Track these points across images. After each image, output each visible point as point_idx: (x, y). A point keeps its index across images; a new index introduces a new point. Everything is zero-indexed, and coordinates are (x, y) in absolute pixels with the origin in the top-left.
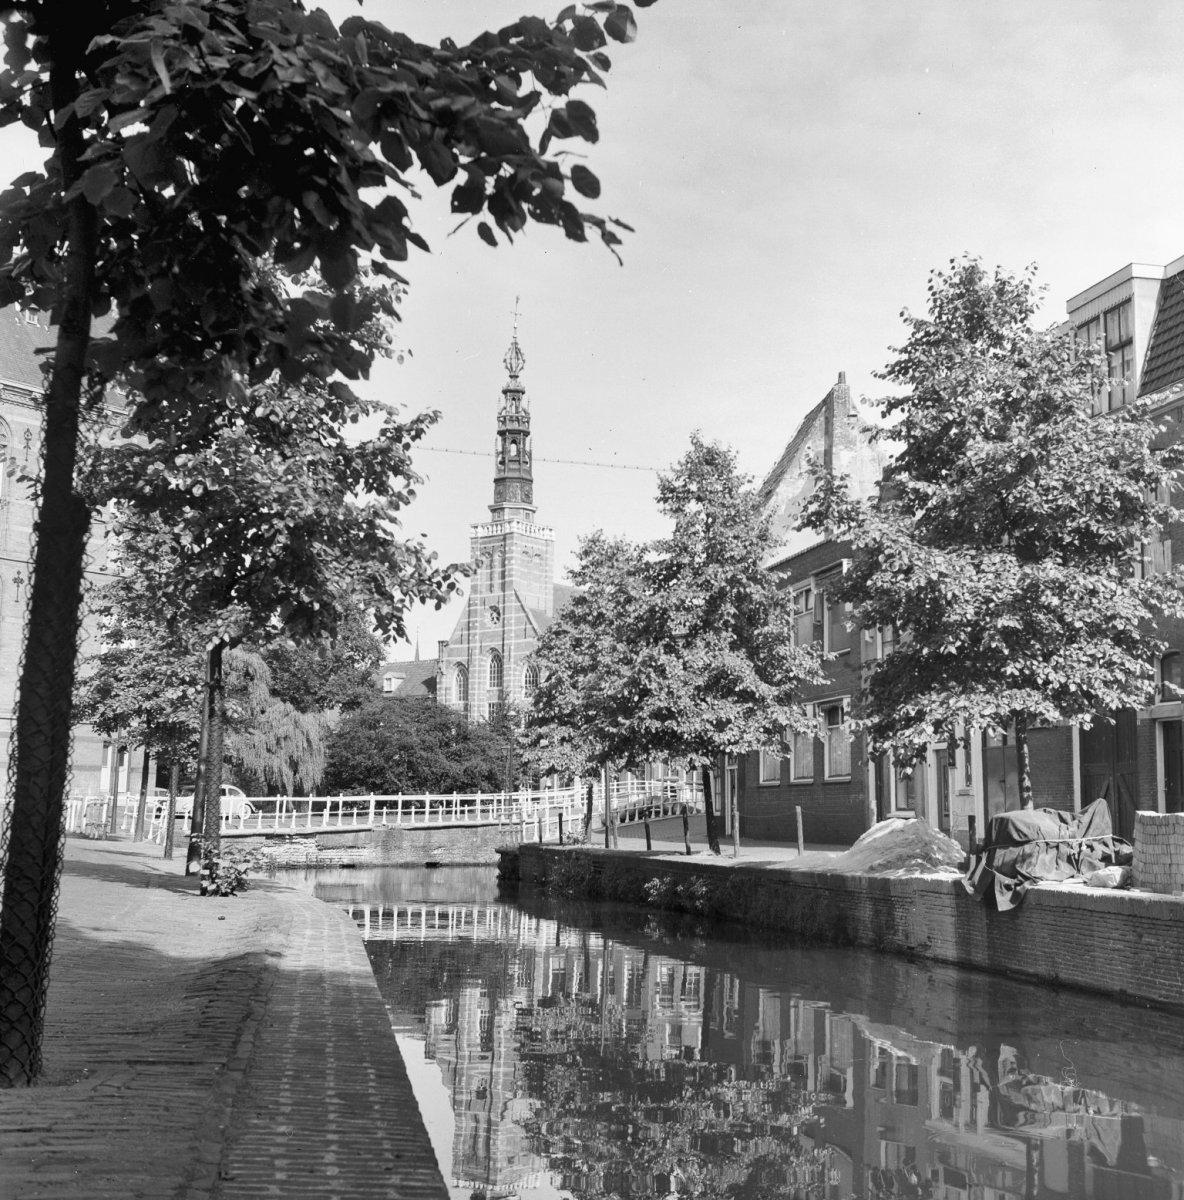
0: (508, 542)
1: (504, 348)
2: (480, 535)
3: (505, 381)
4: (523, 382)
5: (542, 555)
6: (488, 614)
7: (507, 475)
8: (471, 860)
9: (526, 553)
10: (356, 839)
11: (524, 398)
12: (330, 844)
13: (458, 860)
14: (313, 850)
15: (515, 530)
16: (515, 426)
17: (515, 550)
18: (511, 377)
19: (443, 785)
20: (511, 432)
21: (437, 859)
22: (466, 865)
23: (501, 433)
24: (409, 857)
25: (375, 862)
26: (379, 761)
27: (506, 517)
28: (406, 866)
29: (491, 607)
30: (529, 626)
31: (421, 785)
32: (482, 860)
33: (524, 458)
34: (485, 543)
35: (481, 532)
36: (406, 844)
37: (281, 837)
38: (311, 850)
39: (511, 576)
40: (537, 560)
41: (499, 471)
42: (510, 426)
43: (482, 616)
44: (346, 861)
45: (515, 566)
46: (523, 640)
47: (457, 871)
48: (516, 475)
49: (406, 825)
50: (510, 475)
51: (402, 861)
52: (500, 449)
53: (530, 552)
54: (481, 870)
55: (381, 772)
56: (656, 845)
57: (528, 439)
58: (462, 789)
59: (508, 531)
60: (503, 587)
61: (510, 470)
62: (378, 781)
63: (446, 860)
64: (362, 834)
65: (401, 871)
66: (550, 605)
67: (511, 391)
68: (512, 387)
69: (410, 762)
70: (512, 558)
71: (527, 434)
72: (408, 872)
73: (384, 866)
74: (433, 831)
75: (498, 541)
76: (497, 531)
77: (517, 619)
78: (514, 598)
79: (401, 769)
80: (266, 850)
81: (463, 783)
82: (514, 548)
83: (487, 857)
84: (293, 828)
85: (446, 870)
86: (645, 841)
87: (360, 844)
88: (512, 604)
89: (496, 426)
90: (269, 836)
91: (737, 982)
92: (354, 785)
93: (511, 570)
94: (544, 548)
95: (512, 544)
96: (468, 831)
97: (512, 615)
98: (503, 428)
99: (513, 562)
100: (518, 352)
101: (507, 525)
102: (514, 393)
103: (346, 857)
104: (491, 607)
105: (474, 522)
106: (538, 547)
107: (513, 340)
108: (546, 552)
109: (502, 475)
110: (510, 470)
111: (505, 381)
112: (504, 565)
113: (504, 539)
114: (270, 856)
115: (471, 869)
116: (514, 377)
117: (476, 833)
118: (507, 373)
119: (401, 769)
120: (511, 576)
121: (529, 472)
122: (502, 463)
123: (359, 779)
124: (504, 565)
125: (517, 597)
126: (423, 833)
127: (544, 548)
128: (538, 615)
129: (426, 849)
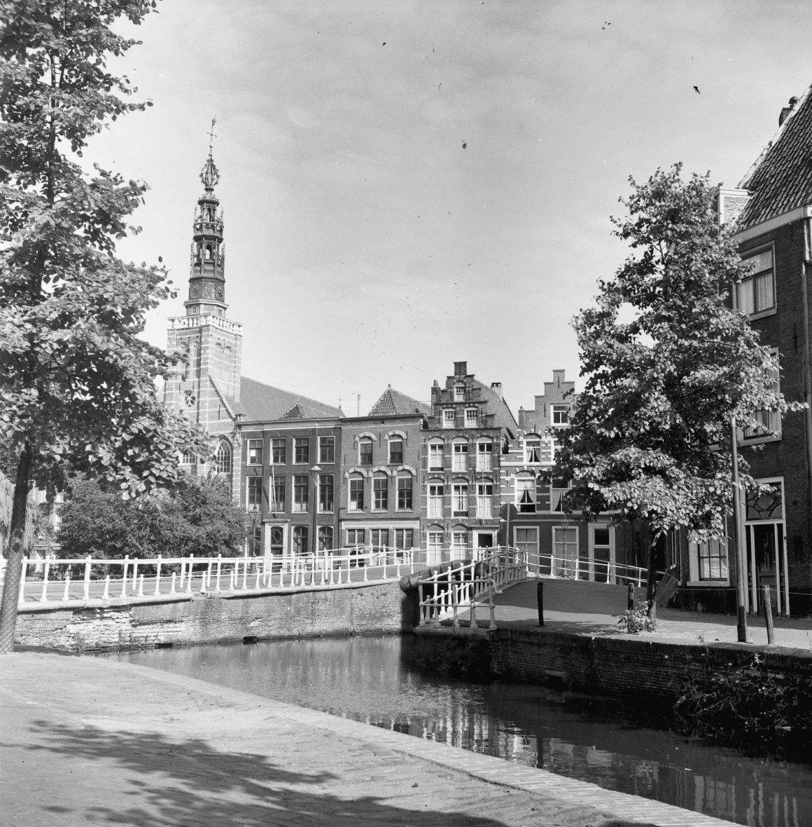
0: (204, 333)
1: (200, 166)
2: (176, 327)
3: (201, 193)
4: (218, 193)
5: (233, 347)
6: (182, 398)
7: (203, 274)
8: (284, 632)
9: (218, 344)
10: (174, 611)
11: (218, 209)
12: (146, 619)
13: (274, 633)
14: (126, 627)
15: (211, 323)
16: (210, 232)
17: (210, 341)
18: (207, 190)
19: (183, 548)
20: (207, 237)
21: (254, 633)
22: (281, 639)
23: (197, 239)
24: (227, 632)
25: (194, 639)
26: (119, 523)
27: (201, 312)
28: (225, 642)
29: (186, 392)
30: (223, 409)
31: (163, 546)
32: (295, 632)
33: (218, 263)
34: (180, 334)
35: (178, 325)
36: (224, 616)
37: (90, 611)
38: (124, 627)
39: (206, 364)
40: (227, 351)
41: (196, 271)
42: (206, 232)
43: (177, 399)
44: (163, 639)
45: (210, 354)
46: (217, 421)
47: (273, 645)
48: (211, 275)
49: (225, 593)
50: (206, 275)
51: (221, 636)
52: (196, 253)
53: (223, 344)
54: (295, 644)
55: (121, 535)
56: (549, 615)
57: (221, 245)
58: (198, 553)
59: (204, 324)
60: (198, 374)
61: (205, 271)
62: (118, 545)
63: (263, 634)
64: (181, 605)
65: (220, 648)
66: (238, 392)
67: (207, 202)
68: (208, 198)
69: (152, 526)
70: (207, 348)
71: (220, 240)
72: (226, 649)
73: (203, 644)
74: (251, 600)
75: (194, 333)
76: (195, 324)
77: (211, 402)
78: (208, 383)
79: (142, 533)
80: (72, 629)
81: (205, 546)
82: (209, 339)
83: (300, 628)
84: (106, 600)
85: (263, 645)
86: (537, 611)
87: (178, 616)
88: (206, 388)
89: (191, 234)
90: (77, 610)
91: (794, 800)
92: (92, 548)
93: (206, 359)
94: (234, 342)
95: (208, 336)
96: (282, 599)
97: (207, 399)
98: (199, 233)
99: (208, 351)
100: (213, 167)
101: (203, 319)
102: (209, 205)
103: (162, 634)
104: (186, 392)
105: (172, 316)
106: (229, 340)
107: (208, 158)
108: (236, 345)
109: (198, 275)
110: (205, 271)
111: (201, 193)
112: (199, 354)
113: (200, 332)
114: (76, 636)
115: (284, 644)
116: (209, 190)
117: (290, 602)
118: (204, 186)
119: (142, 533)
120: (206, 364)
121: (222, 274)
122: (198, 264)
123: (97, 543)
124: (199, 354)
125: (212, 382)
126: (240, 601)
127: (234, 342)
128: (231, 400)
129: (244, 621)
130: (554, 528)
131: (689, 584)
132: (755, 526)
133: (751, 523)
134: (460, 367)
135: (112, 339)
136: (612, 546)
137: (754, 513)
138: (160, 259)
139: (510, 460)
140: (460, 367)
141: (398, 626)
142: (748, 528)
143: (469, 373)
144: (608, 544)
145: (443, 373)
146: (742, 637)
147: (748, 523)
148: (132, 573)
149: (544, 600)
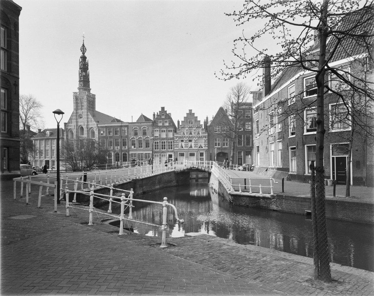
4: (86, 55)
130: (178, 153)
131: (305, 175)
132: (336, 157)
133: (335, 157)
134: (163, 108)
135: (293, 120)
136: (204, 157)
137: (335, 153)
138: (243, 78)
139: (177, 134)
140: (163, 108)
141: (56, 170)
142: (333, 158)
143: (165, 110)
144: (203, 156)
145: (158, 110)
146: (348, 194)
147: (333, 156)
148: (108, 197)
149: (244, 183)
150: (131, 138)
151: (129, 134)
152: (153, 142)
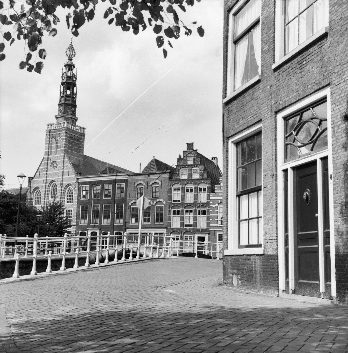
4: (74, 61)
150: (130, 204)
151: (128, 195)
152: (170, 211)
